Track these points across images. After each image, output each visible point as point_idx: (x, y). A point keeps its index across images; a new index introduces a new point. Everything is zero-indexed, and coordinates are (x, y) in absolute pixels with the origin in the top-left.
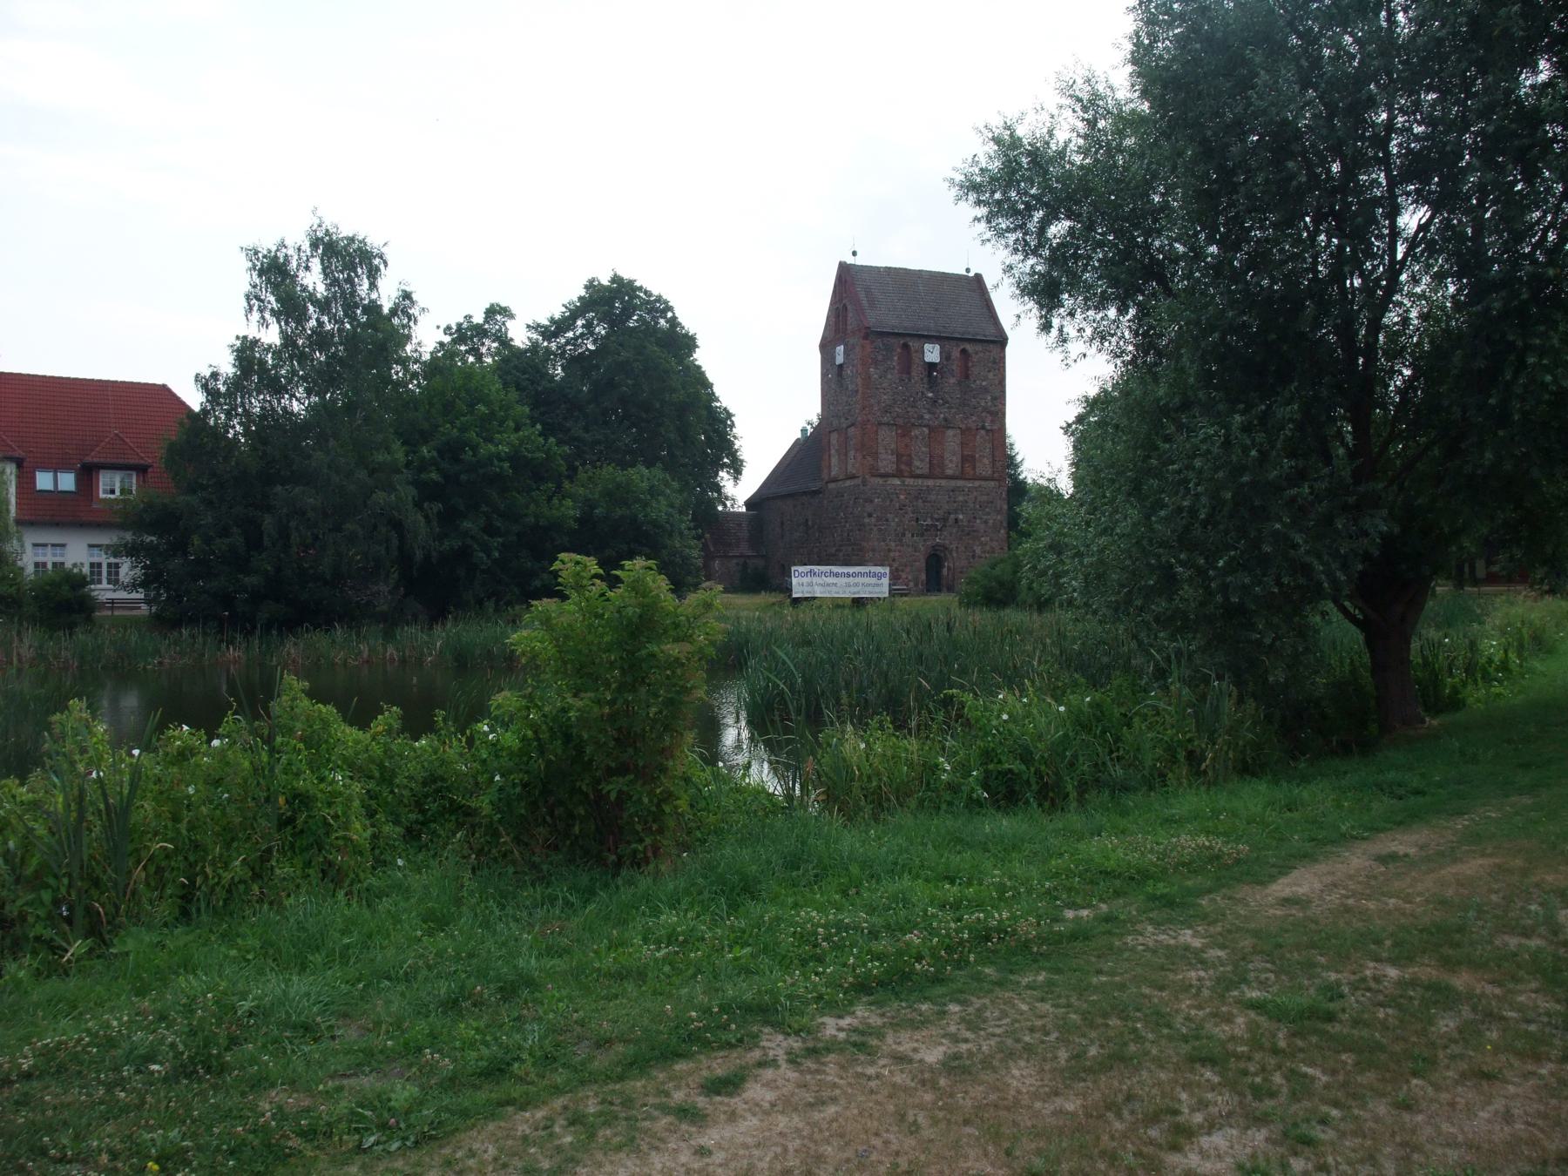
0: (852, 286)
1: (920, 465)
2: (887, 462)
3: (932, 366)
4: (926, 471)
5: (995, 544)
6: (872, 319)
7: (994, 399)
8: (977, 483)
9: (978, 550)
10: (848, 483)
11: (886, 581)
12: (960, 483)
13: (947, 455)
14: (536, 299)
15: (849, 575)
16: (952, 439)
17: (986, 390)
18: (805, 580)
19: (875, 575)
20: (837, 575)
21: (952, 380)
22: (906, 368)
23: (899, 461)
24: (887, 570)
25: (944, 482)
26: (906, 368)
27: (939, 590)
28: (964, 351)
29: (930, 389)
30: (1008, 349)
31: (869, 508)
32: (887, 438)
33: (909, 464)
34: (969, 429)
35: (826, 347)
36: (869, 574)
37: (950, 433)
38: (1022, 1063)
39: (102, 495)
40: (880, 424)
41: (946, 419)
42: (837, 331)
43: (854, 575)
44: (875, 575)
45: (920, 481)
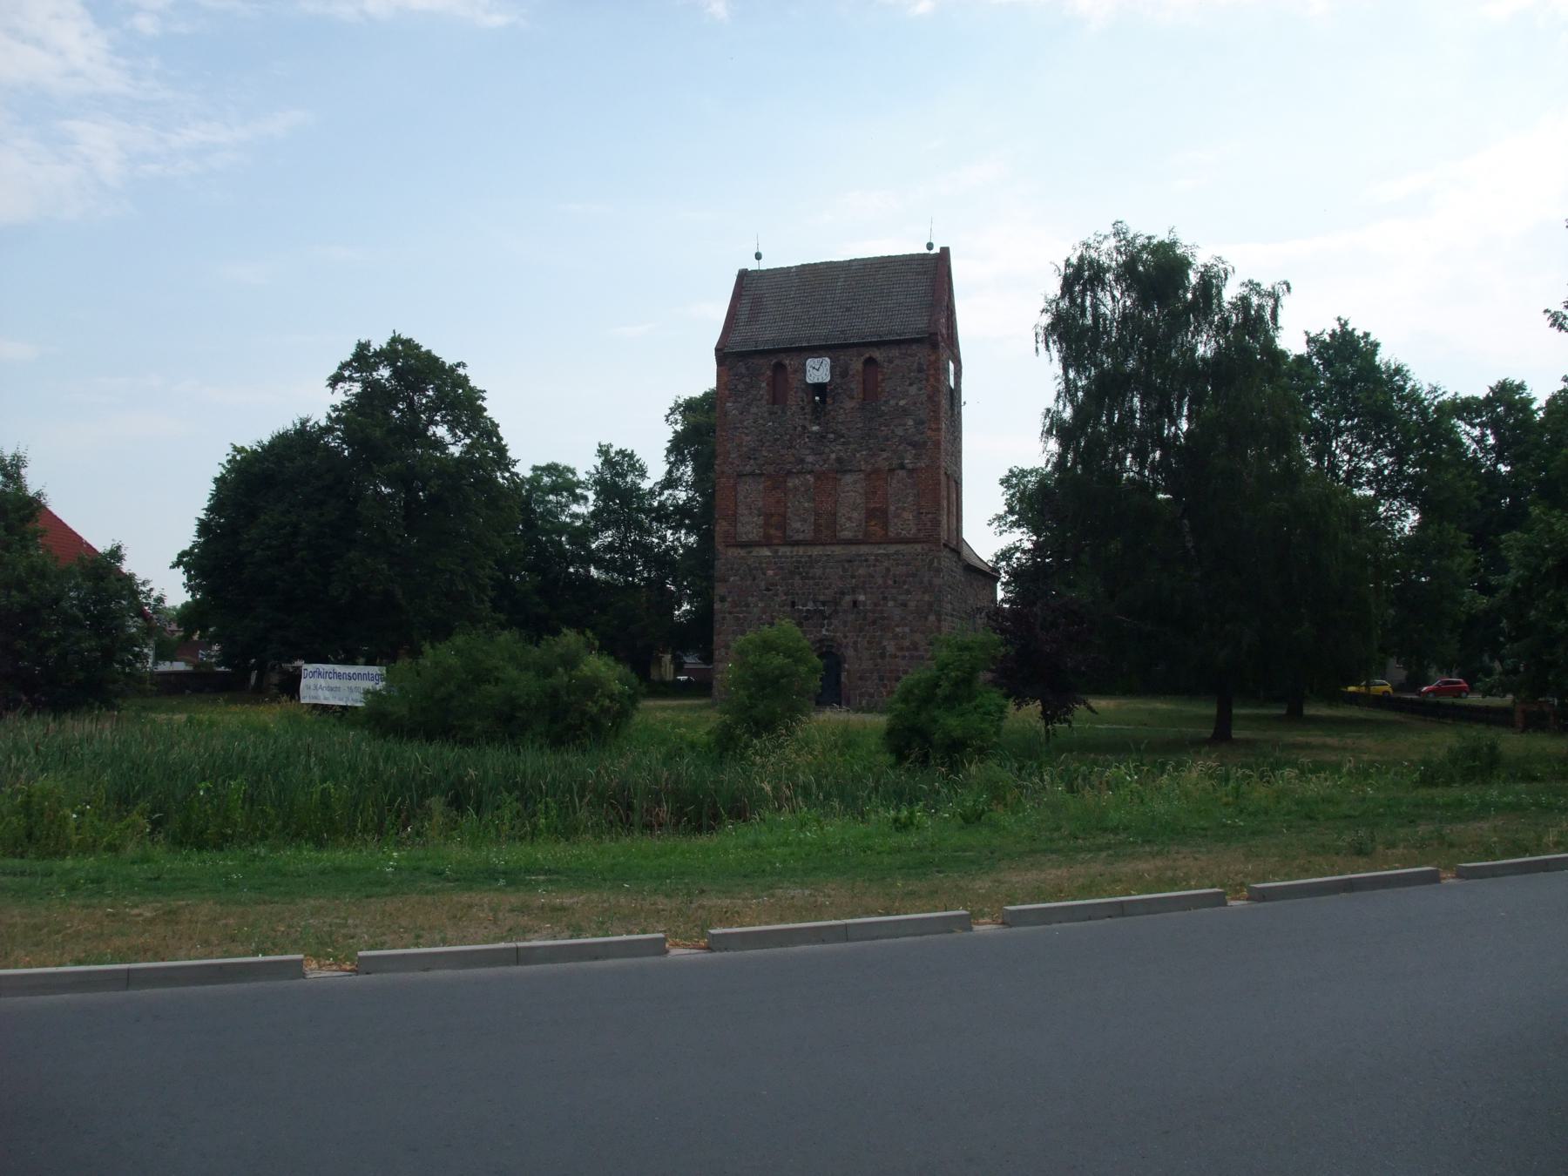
3: (819, 388)
4: (809, 535)
5: (917, 637)
8: (892, 549)
9: (891, 648)
12: (864, 549)
16: (851, 489)
21: (849, 404)
23: (767, 524)
26: (777, 397)
28: (870, 361)
33: (783, 526)
34: (876, 471)
37: (849, 478)
40: (740, 475)
41: (839, 460)
45: (801, 550)
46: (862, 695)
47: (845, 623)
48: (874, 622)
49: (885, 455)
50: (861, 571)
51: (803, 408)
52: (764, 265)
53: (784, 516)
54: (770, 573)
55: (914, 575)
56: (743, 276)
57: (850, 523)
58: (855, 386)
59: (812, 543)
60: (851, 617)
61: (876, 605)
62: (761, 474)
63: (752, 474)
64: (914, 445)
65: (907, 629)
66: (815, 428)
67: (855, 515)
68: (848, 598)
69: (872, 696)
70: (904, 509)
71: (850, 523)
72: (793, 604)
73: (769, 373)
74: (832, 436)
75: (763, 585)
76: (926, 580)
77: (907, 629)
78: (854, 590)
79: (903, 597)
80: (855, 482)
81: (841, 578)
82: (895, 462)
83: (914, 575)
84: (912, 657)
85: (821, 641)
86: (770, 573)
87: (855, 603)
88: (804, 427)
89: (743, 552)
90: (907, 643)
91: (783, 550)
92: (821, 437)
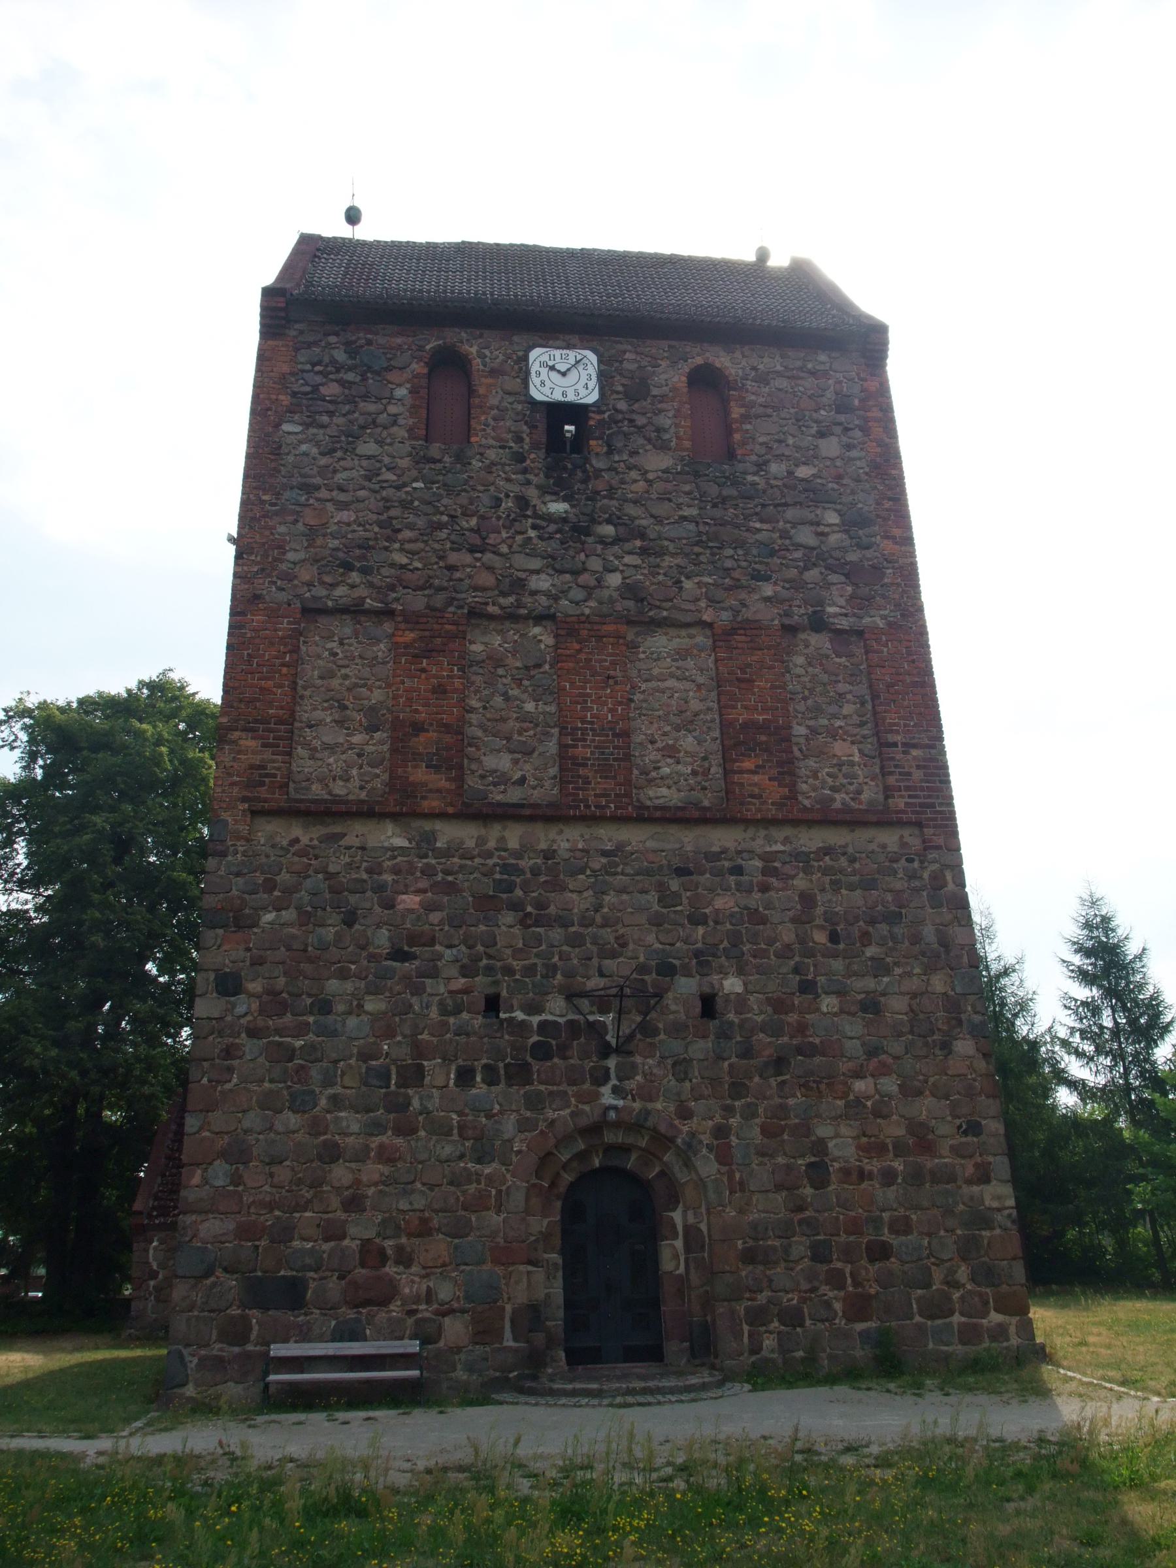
4: (544, 790)
5: (925, 1107)
7: (853, 523)
8: (811, 840)
9: (842, 1145)
12: (723, 838)
13: (643, 730)
16: (671, 675)
21: (657, 462)
23: (400, 751)
25: (635, 837)
27: (653, 1354)
28: (705, 380)
29: (559, 488)
33: (453, 758)
34: (750, 627)
37: (660, 643)
40: (312, 612)
41: (630, 590)
45: (513, 835)
46: (758, 1317)
47: (681, 1068)
48: (779, 1063)
49: (768, 590)
50: (724, 903)
51: (520, 458)
52: (364, 232)
53: (457, 730)
54: (409, 901)
55: (893, 918)
57: (676, 760)
59: (551, 815)
60: (700, 1048)
61: (780, 1006)
62: (390, 613)
63: (354, 610)
64: (851, 573)
65: (890, 1084)
66: (558, 507)
67: (688, 742)
68: (687, 986)
69: (793, 1318)
70: (833, 734)
71: (676, 760)
72: (492, 1005)
73: (418, 367)
74: (609, 530)
75: (382, 939)
76: (929, 932)
77: (890, 1084)
78: (703, 961)
79: (870, 983)
80: (682, 654)
81: (657, 922)
82: (799, 613)
83: (893, 918)
84: (916, 1177)
85: (594, 1130)
86: (409, 901)
87: (709, 1005)
88: (523, 502)
89: (304, 834)
90: (894, 1130)
91: (448, 833)
92: (577, 531)
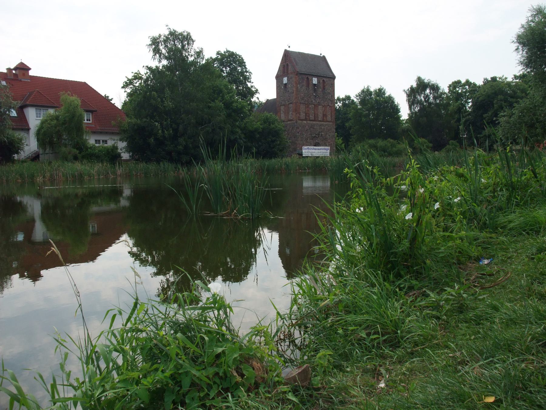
0: (288, 57)
1: (312, 117)
2: (303, 116)
3: (315, 85)
4: (313, 119)
6: (298, 69)
7: (332, 96)
8: (327, 123)
10: (289, 122)
11: (329, 151)
12: (323, 123)
14: (144, 62)
15: (318, 149)
17: (329, 93)
18: (307, 151)
19: (326, 149)
20: (315, 149)
22: (308, 85)
24: (329, 148)
25: (318, 122)
26: (308, 85)
28: (323, 81)
29: (314, 92)
30: (335, 80)
31: (298, 130)
32: (302, 108)
33: (309, 117)
35: (279, 78)
36: (324, 149)
37: (320, 107)
38: (181, 321)
39: (86, 121)
42: (284, 72)
43: (320, 149)
44: (326, 149)
56: (286, 51)
58: (321, 86)
